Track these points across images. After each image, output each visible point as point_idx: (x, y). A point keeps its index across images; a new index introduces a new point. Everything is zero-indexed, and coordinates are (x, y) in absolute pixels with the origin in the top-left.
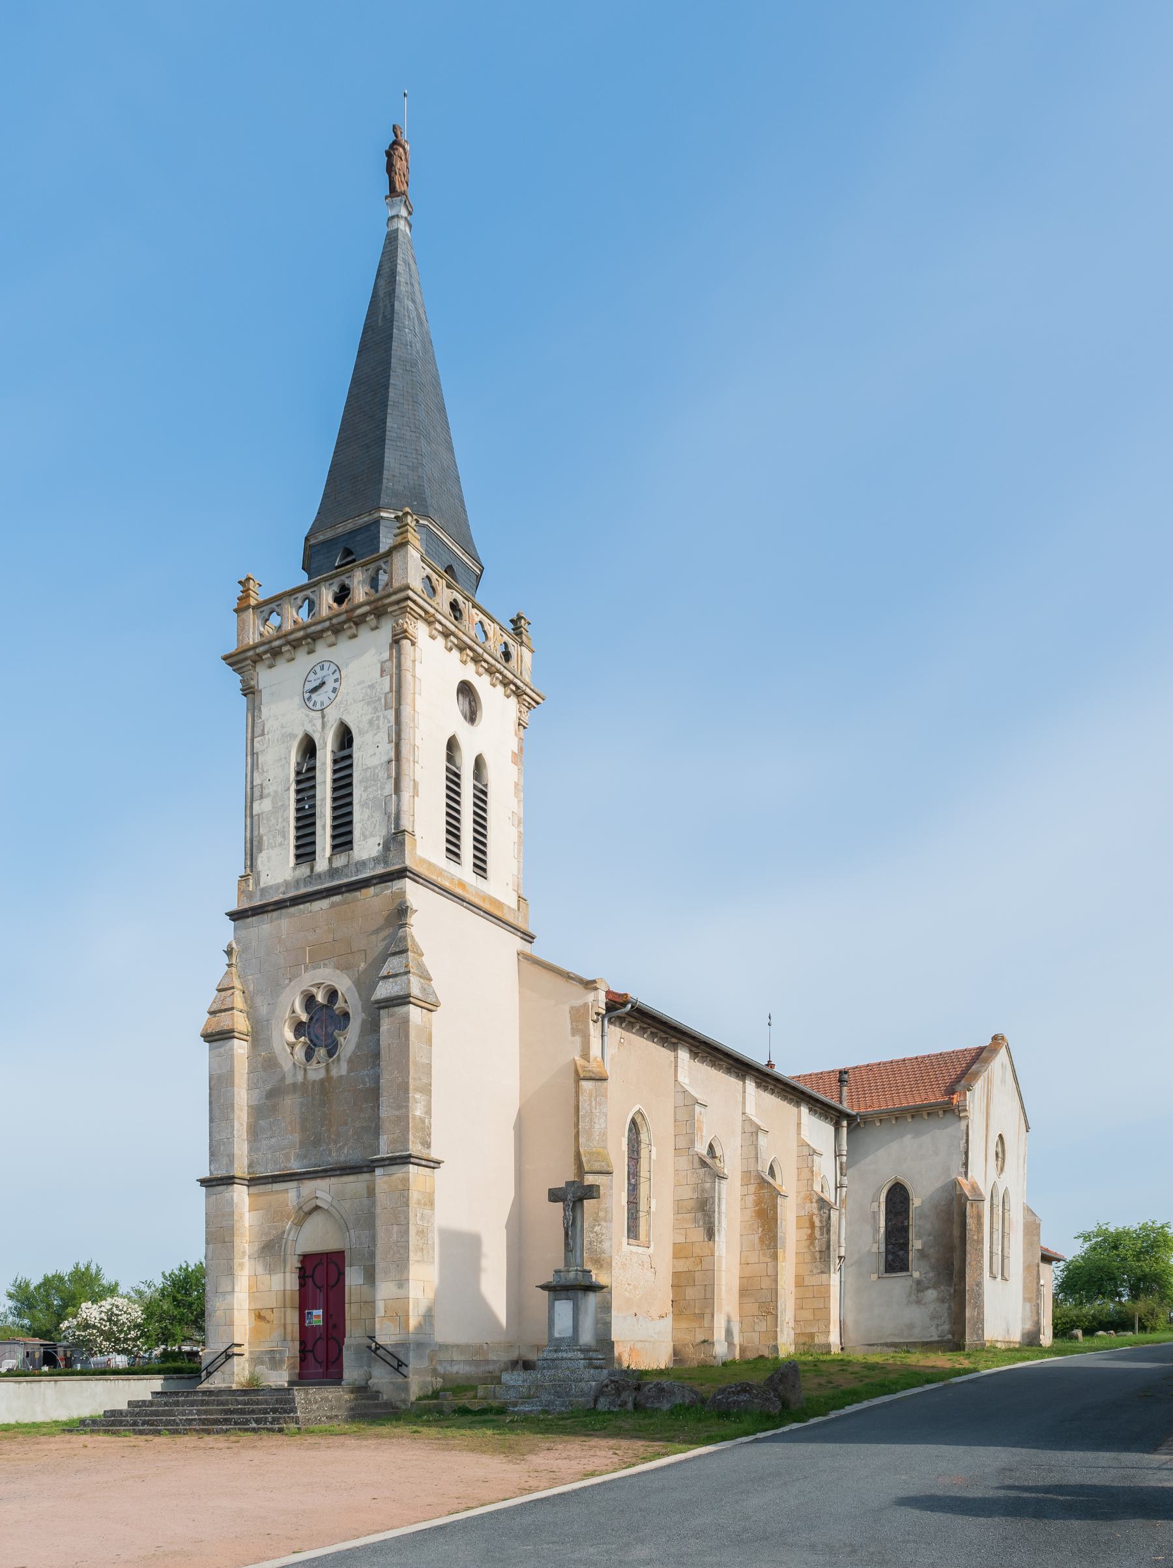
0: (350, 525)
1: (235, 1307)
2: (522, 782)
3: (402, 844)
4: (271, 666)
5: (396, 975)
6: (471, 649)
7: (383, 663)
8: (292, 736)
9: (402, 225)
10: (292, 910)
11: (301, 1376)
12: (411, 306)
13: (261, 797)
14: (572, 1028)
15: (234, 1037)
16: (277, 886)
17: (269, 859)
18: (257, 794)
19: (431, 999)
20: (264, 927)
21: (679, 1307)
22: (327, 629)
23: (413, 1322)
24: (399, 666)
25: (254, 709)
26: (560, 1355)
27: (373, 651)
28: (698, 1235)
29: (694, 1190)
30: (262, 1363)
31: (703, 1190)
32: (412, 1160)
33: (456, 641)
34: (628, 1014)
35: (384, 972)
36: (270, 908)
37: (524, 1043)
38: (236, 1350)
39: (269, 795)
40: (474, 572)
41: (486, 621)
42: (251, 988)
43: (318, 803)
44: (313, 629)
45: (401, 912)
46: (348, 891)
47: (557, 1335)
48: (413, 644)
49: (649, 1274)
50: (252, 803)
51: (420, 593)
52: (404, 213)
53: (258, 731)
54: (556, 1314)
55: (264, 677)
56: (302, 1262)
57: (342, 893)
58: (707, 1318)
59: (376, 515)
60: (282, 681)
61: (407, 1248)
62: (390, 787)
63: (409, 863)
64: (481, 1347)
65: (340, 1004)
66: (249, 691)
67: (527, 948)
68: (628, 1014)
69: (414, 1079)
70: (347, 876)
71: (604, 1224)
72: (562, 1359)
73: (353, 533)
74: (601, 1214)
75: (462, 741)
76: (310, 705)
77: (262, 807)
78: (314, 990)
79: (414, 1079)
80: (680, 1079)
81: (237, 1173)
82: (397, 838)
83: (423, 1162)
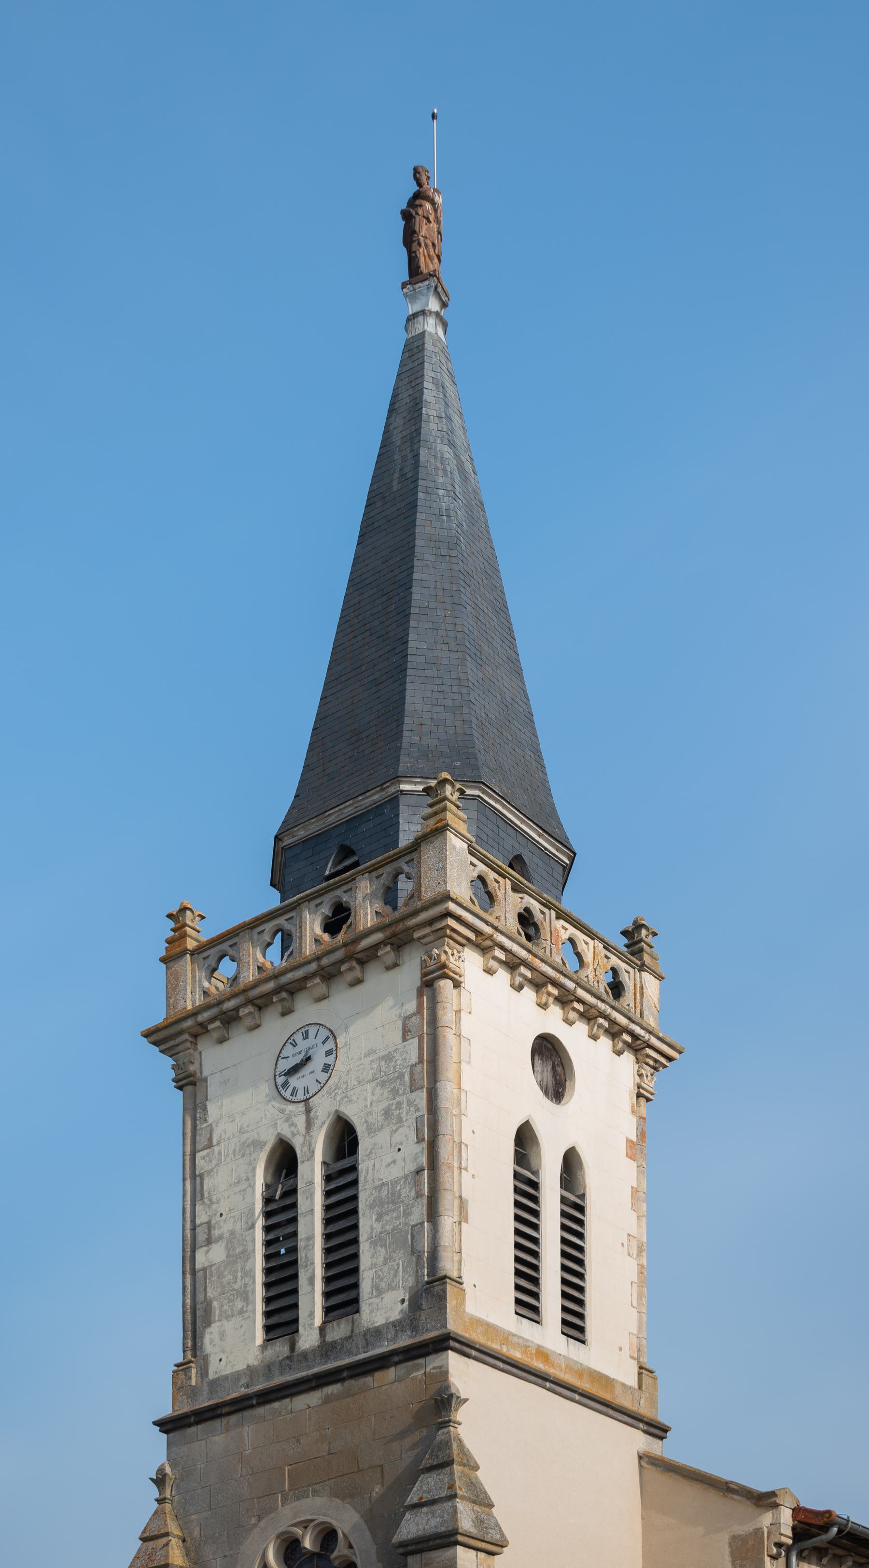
0: (349, 810)
3: (442, 1298)
4: (221, 1041)
5: (433, 1502)
7: (406, 1019)
8: (258, 1144)
9: (431, 326)
10: (261, 1411)
13: (209, 1242)
16: (236, 1377)
17: (222, 1335)
18: (201, 1237)
19: (495, 1536)
20: (216, 1439)
22: (313, 975)
24: (434, 1021)
27: (390, 1002)
33: (528, 974)
35: (413, 1498)
39: (220, 1238)
40: (558, 861)
41: (580, 937)
42: (196, 1533)
43: (301, 1244)
44: (290, 976)
45: (442, 1403)
46: (351, 1377)
48: (457, 985)
50: (193, 1251)
52: (434, 305)
53: (202, 1141)
55: (212, 1059)
57: (342, 1380)
59: (392, 790)
62: (419, 1211)
63: (453, 1325)
65: (340, 1551)
66: (188, 1082)
67: (656, 1447)
70: (350, 1353)
73: (353, 822)
76: (287, 1094)
77: (210, 1256)
78: (299, 1531)
82: (433, 1288)
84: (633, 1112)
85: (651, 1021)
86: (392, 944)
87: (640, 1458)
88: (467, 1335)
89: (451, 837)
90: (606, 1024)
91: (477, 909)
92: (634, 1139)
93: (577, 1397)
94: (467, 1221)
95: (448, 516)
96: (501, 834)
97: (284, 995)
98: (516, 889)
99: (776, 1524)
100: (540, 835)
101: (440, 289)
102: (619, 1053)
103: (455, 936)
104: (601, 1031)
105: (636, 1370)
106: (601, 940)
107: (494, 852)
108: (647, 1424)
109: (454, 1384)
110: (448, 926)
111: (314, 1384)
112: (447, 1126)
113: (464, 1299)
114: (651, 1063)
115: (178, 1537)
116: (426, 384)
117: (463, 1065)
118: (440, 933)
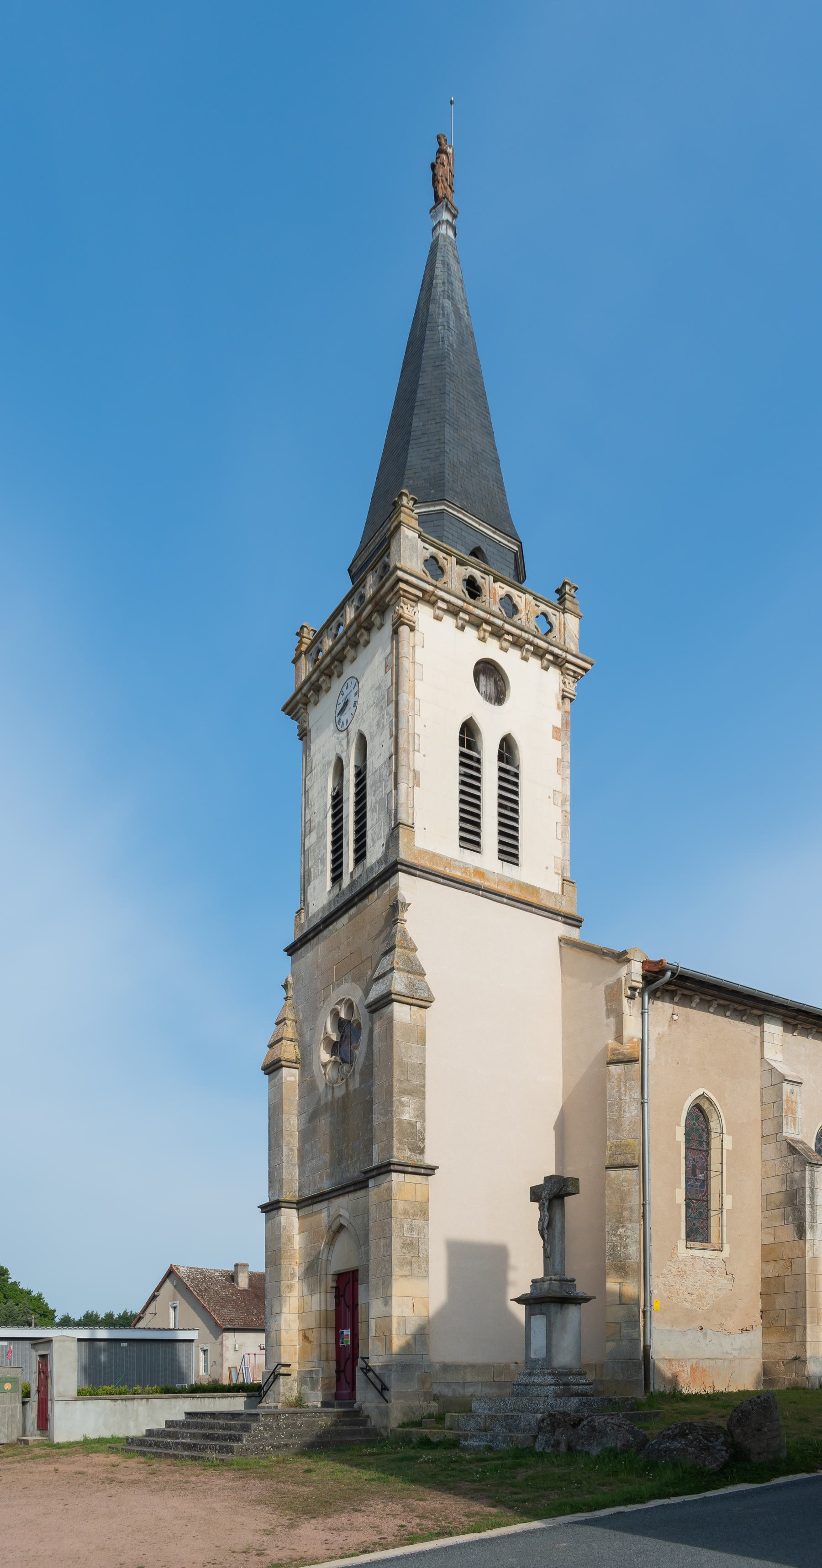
1: (283, 1327)
2: (568, 757)
6: (488, 623)
11: (337, 1396)
12: (447, 303)
14: (607, 1010)
15: (282, 1066)
19: (423, 994)
21: (770, 1318)
23: (397, 1343)
25: (306, 749)
26: (536, 1379)
28: (787, 1233)
29: (783, 1182)
30: (305, 1383)
31: (792, 1181)
32: (392, 1167)
33: (467, 617)
34: (670, 984)
36: (311, 936)
37: (566, 1035)
38: (283, 1370)
40: (510, 550)
47: (533, 1356)
48: (412, 629)
49: (724, 1281)
51: (423, 576)
52: (446, 216)
53: (309, 769)
54: (532, 1332)
56: (338, 1281)
58: (799, 1330)
60: (321, 714)
61: (390, 1262)
62: (391, 783)
63: (404, 855)
64: (507, 1367)
67: (574, 933)
68: (670, 984)
69: (401, 1081)
71: (629, 1225)
72: (534, 1384)
74: (626, 1214)
75: (481, 723)
76: (340, 727)
77: (311, 840)
79: (401, 1081)
80: (768, 1055)
81: (286, 1196)
83: (410, 1169)
84: (559, 708)
85: (573, 647)
86: (378, 611)
87: (560, 940)
88: (416, 862)
89: (404, 530)
90: (532, 648)
91: (430, 579)
92: (560, 726)
93: (505, 900)
94: (418, 785)
95: (443, 341)
96: (463, 533)
97: (336, 663)
98: (460, 563)
99: (629, 974)
100: (494, 533)
101: (450, 206)
102: (546, 669)
103: (407, 595)
104: (529, 654)
105: (560, 882)
106: (531, 594)
107: (458, 546)
108: (565, 917)
109: (401, 895)
110: (400, 589)
111: (344, 909)
112: (402, 725)
113: (414, 837)
114: (572, 674)
115: (293, 1020)
116: (437, 265)
117: (417, 682)
118: (398, 595)
